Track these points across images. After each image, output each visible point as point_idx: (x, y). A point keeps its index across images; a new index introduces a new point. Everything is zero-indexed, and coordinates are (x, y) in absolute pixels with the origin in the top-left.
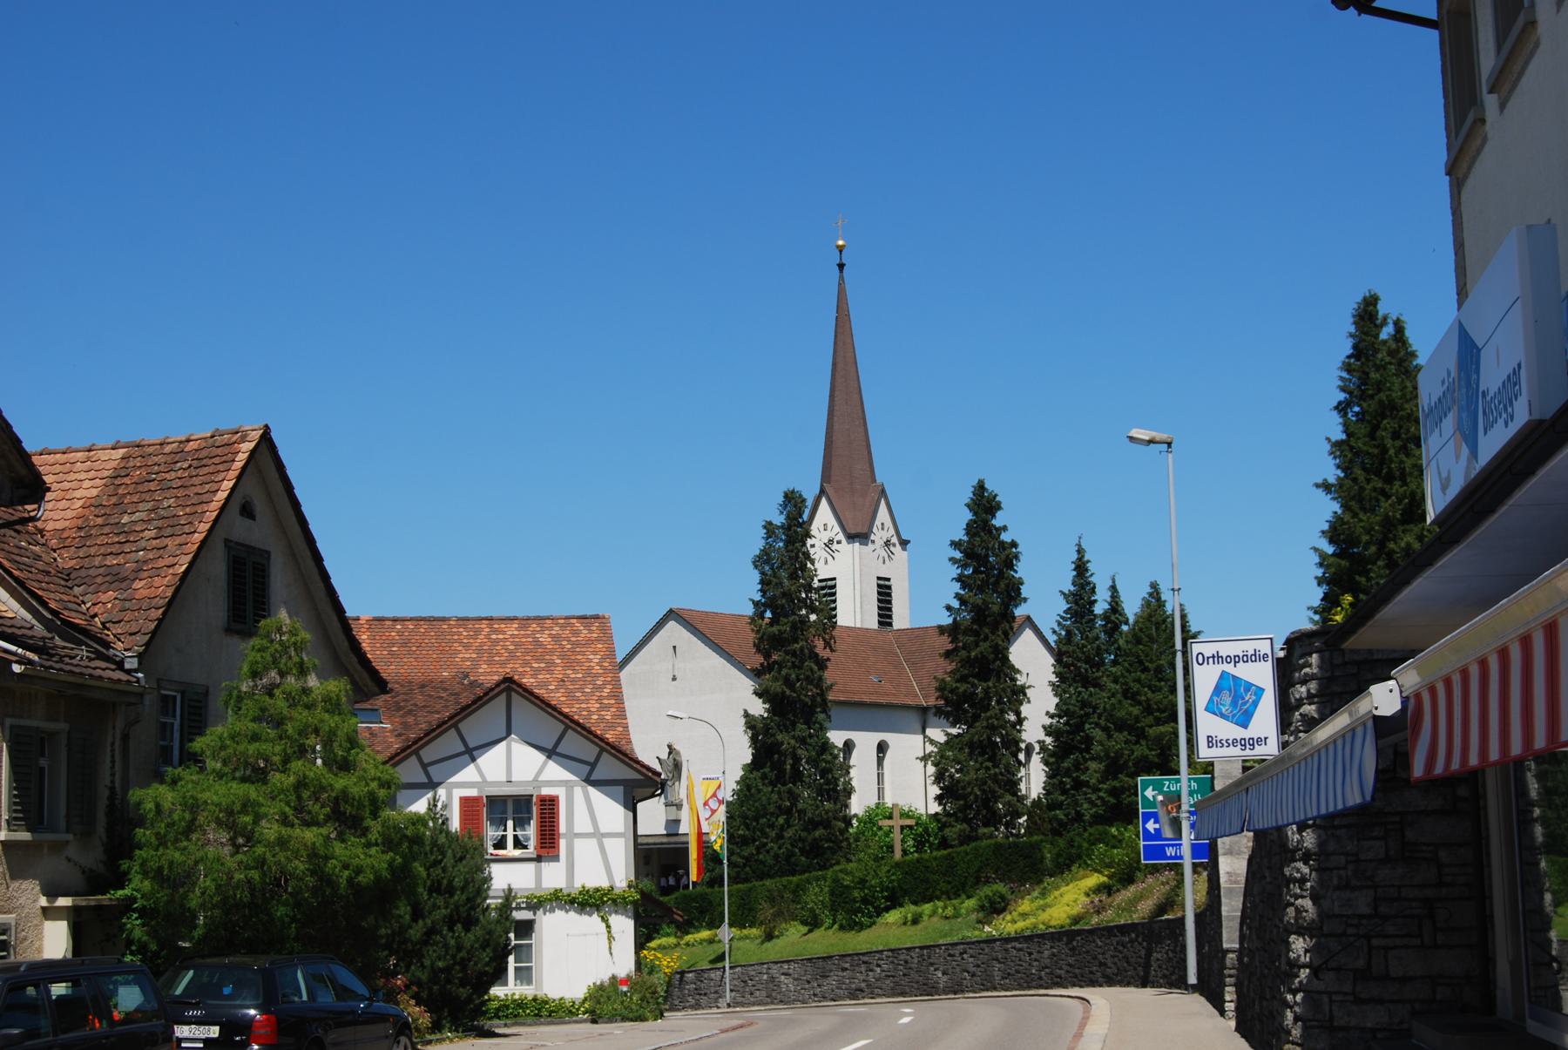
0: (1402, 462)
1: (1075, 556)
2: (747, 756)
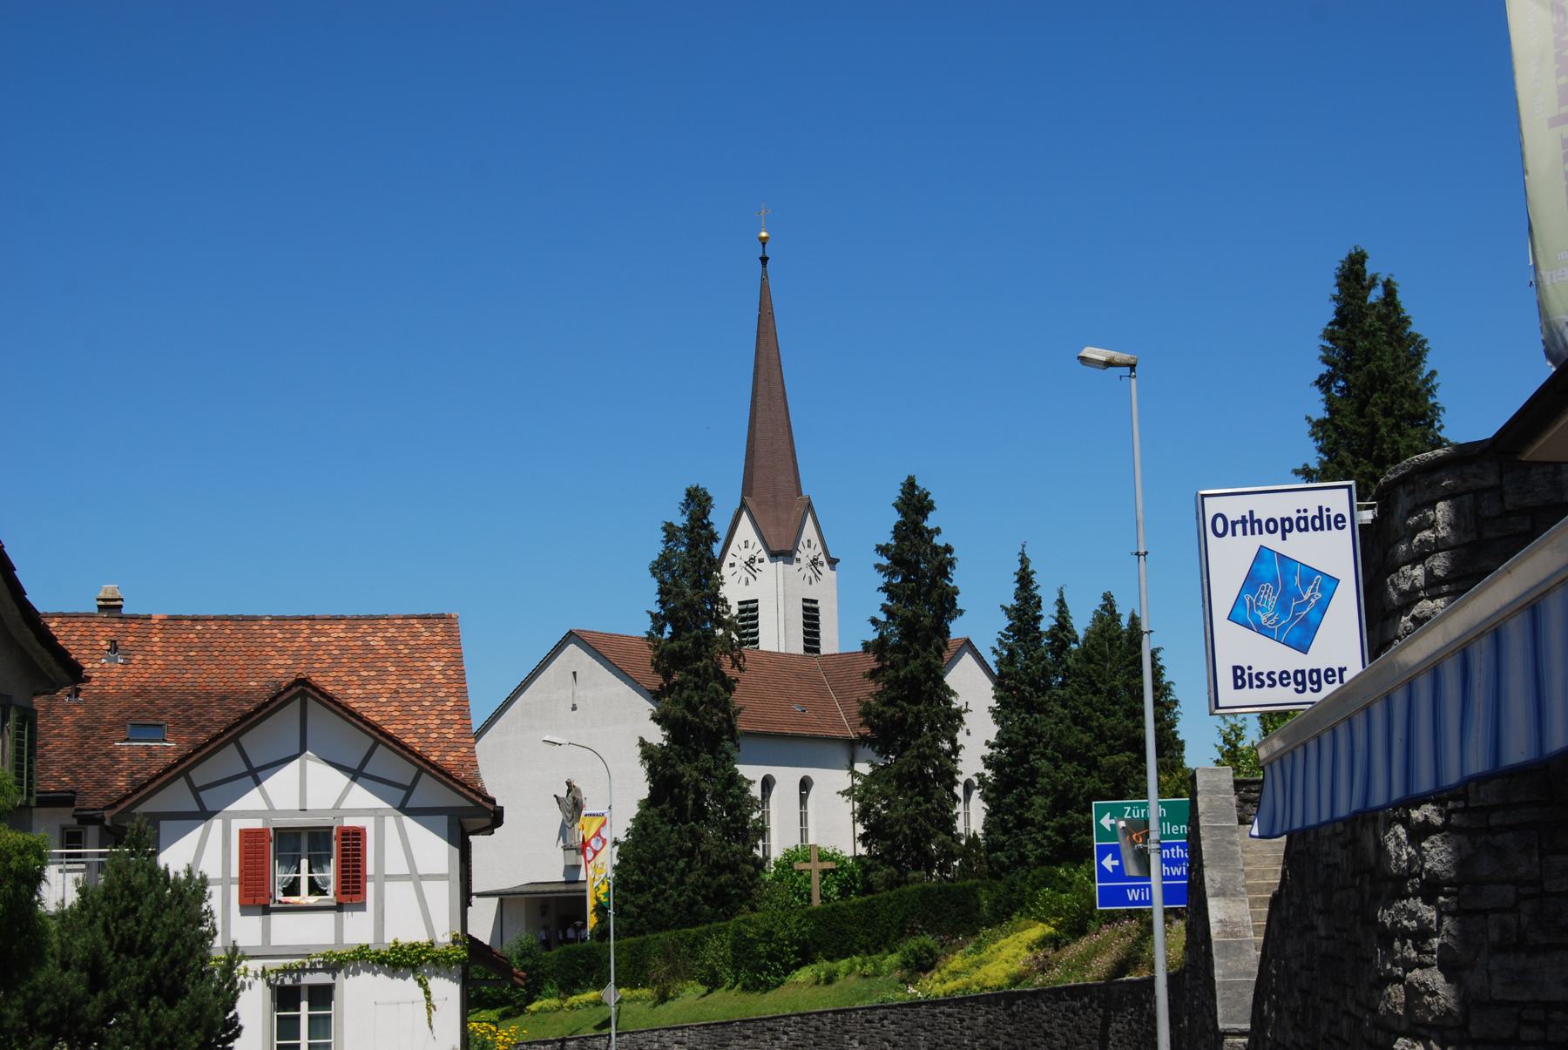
0: (1395, 442)
1: (1018, 567)
2: (643, 790)
